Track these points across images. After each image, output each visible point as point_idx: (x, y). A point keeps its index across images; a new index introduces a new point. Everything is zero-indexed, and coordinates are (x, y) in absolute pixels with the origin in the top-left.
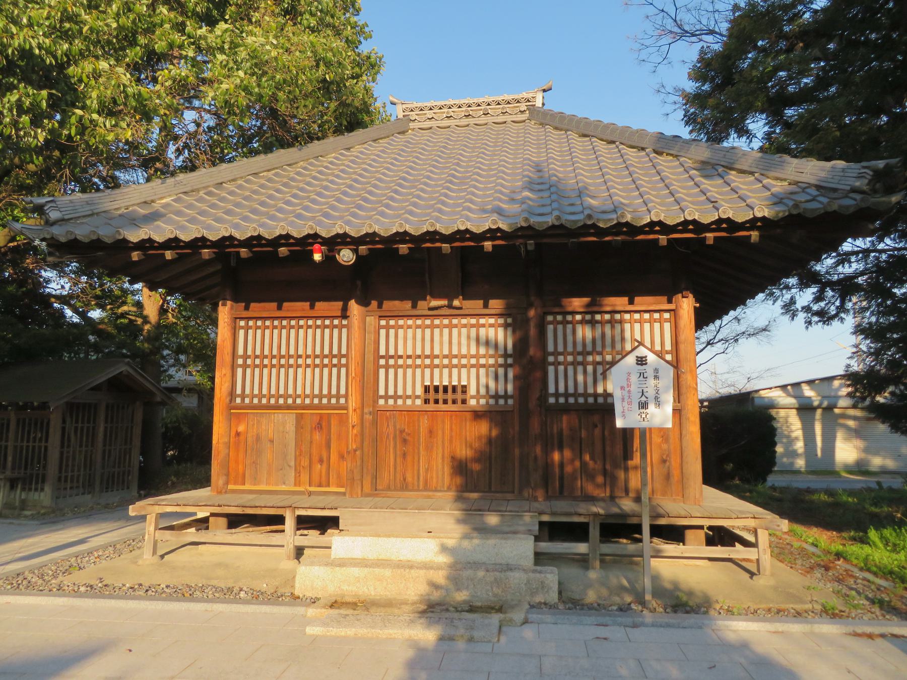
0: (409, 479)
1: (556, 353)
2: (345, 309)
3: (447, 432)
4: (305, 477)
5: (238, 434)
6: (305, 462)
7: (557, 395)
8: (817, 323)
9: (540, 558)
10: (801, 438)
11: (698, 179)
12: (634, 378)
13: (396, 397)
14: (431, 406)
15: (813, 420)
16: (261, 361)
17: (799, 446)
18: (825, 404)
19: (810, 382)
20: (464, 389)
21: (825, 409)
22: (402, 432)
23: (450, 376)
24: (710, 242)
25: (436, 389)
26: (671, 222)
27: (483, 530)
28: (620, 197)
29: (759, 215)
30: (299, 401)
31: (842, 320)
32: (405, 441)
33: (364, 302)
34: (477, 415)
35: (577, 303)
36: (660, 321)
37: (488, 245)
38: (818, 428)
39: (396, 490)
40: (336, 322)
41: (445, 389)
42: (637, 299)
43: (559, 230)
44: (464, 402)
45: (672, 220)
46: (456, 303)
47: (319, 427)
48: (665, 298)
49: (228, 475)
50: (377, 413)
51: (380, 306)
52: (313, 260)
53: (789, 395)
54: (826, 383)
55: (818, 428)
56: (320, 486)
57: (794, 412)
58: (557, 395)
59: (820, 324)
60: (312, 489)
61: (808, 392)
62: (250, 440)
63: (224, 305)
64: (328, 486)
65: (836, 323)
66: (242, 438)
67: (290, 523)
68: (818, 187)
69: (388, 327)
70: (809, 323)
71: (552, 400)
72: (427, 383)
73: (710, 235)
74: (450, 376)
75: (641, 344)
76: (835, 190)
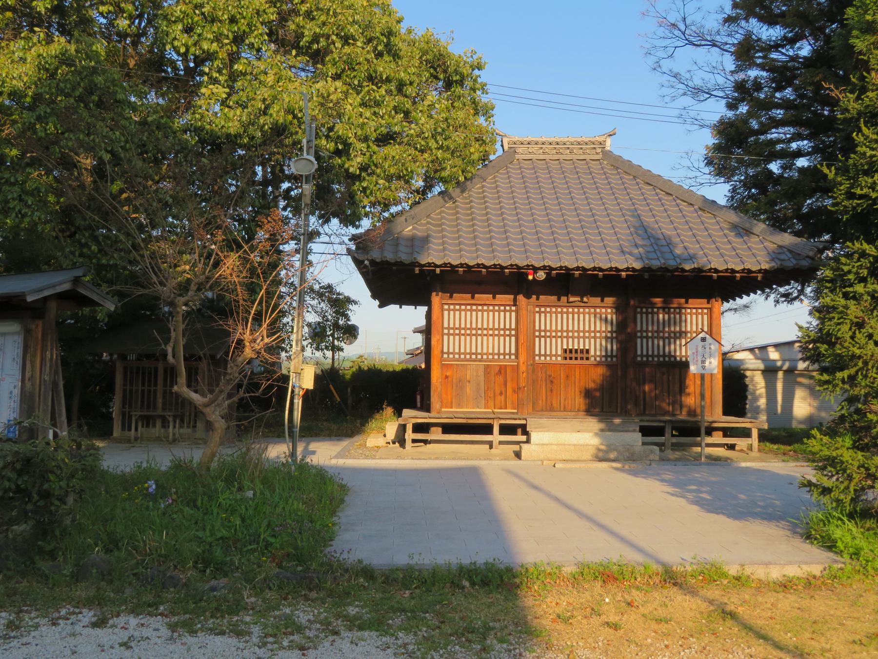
0: (555, 405)
1: (641, 331)
2: (515, 300)
3: (577, 377)
4: (491, 403)
5: (447, 377)
6: (491, 394)
7: (642, 356)
8: (783, 302)
9: (644, 444)
10: (764, 395)
11: (726, 231)
12: (700, 349)
13: (551, 355)
14: (568, 361)
15: (776, 379)
16: (460, 332)
17: (762, 402)
18: (786, 366)
19: (777, 346)
20: (588, 351)
21: (786, 372)
22: (550, 376)
23: (579, 343)
24: (738, 279)
25: (571, 351)
26: (720, 269)
27: (611, 428)
28: (693, 248)
29: (763, 268)
30: (485, 357)
31: (802, 300)
32: (552, 382)
33: (528, 297)
34: (599, 364)
35: (658, 300)
36: (702, 314)
37: (624, 274)
38: (780, 386)
39: (546, 411)
40: (508, 308)
41: (576, 351)
42: (690, 301)
43: (664, 270)
44: (587, 359)
45: (721, 268)
46: (585, 299)
47: (500, 372)
48: (706, 300)
49: (442, 402)
50: (534, 364)
51: (538, 299)
52: (529, 280)
53: (757, 358)
54: (787, 347)
55: (780, 386)
56: (501, 408)
57: (760, 372)
58: (642, 356)
59: (785, 303)
60: (496, 410)
61: (774, 355)
62: (454, 380)
63: (437, 295)
64: (506, 408)
65: (797, 303)
66: (450, 379)
67: (496, 429)
68: (790, 251)
69: (540, 312)
70: (777, 302)
71: (639, 359)
72: (565, 347)
73: (738, 275)
74: (579, 343)
75: (703, 331)
76: (799, 255)
